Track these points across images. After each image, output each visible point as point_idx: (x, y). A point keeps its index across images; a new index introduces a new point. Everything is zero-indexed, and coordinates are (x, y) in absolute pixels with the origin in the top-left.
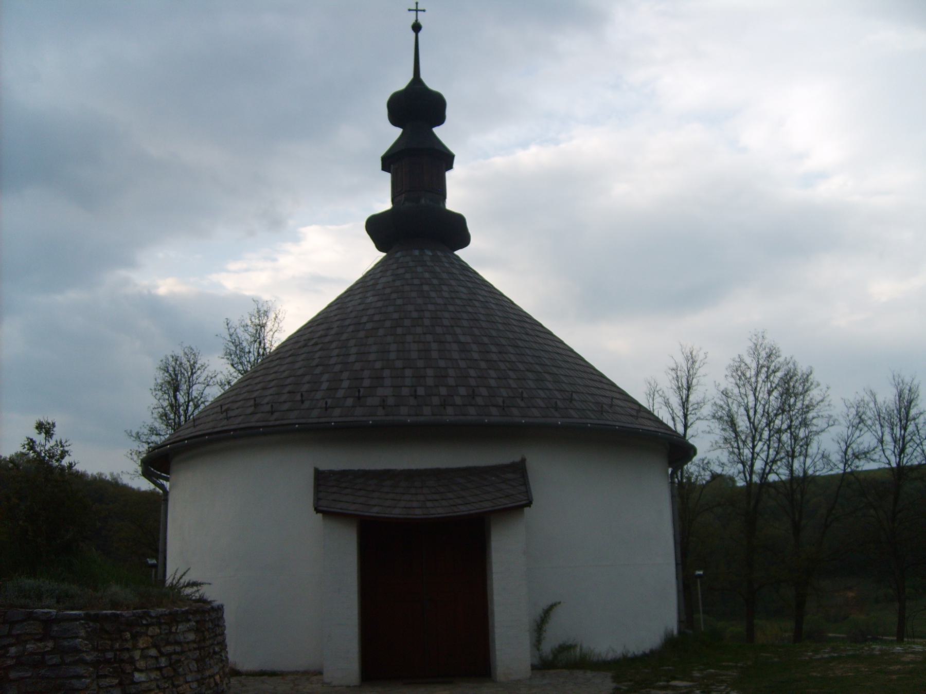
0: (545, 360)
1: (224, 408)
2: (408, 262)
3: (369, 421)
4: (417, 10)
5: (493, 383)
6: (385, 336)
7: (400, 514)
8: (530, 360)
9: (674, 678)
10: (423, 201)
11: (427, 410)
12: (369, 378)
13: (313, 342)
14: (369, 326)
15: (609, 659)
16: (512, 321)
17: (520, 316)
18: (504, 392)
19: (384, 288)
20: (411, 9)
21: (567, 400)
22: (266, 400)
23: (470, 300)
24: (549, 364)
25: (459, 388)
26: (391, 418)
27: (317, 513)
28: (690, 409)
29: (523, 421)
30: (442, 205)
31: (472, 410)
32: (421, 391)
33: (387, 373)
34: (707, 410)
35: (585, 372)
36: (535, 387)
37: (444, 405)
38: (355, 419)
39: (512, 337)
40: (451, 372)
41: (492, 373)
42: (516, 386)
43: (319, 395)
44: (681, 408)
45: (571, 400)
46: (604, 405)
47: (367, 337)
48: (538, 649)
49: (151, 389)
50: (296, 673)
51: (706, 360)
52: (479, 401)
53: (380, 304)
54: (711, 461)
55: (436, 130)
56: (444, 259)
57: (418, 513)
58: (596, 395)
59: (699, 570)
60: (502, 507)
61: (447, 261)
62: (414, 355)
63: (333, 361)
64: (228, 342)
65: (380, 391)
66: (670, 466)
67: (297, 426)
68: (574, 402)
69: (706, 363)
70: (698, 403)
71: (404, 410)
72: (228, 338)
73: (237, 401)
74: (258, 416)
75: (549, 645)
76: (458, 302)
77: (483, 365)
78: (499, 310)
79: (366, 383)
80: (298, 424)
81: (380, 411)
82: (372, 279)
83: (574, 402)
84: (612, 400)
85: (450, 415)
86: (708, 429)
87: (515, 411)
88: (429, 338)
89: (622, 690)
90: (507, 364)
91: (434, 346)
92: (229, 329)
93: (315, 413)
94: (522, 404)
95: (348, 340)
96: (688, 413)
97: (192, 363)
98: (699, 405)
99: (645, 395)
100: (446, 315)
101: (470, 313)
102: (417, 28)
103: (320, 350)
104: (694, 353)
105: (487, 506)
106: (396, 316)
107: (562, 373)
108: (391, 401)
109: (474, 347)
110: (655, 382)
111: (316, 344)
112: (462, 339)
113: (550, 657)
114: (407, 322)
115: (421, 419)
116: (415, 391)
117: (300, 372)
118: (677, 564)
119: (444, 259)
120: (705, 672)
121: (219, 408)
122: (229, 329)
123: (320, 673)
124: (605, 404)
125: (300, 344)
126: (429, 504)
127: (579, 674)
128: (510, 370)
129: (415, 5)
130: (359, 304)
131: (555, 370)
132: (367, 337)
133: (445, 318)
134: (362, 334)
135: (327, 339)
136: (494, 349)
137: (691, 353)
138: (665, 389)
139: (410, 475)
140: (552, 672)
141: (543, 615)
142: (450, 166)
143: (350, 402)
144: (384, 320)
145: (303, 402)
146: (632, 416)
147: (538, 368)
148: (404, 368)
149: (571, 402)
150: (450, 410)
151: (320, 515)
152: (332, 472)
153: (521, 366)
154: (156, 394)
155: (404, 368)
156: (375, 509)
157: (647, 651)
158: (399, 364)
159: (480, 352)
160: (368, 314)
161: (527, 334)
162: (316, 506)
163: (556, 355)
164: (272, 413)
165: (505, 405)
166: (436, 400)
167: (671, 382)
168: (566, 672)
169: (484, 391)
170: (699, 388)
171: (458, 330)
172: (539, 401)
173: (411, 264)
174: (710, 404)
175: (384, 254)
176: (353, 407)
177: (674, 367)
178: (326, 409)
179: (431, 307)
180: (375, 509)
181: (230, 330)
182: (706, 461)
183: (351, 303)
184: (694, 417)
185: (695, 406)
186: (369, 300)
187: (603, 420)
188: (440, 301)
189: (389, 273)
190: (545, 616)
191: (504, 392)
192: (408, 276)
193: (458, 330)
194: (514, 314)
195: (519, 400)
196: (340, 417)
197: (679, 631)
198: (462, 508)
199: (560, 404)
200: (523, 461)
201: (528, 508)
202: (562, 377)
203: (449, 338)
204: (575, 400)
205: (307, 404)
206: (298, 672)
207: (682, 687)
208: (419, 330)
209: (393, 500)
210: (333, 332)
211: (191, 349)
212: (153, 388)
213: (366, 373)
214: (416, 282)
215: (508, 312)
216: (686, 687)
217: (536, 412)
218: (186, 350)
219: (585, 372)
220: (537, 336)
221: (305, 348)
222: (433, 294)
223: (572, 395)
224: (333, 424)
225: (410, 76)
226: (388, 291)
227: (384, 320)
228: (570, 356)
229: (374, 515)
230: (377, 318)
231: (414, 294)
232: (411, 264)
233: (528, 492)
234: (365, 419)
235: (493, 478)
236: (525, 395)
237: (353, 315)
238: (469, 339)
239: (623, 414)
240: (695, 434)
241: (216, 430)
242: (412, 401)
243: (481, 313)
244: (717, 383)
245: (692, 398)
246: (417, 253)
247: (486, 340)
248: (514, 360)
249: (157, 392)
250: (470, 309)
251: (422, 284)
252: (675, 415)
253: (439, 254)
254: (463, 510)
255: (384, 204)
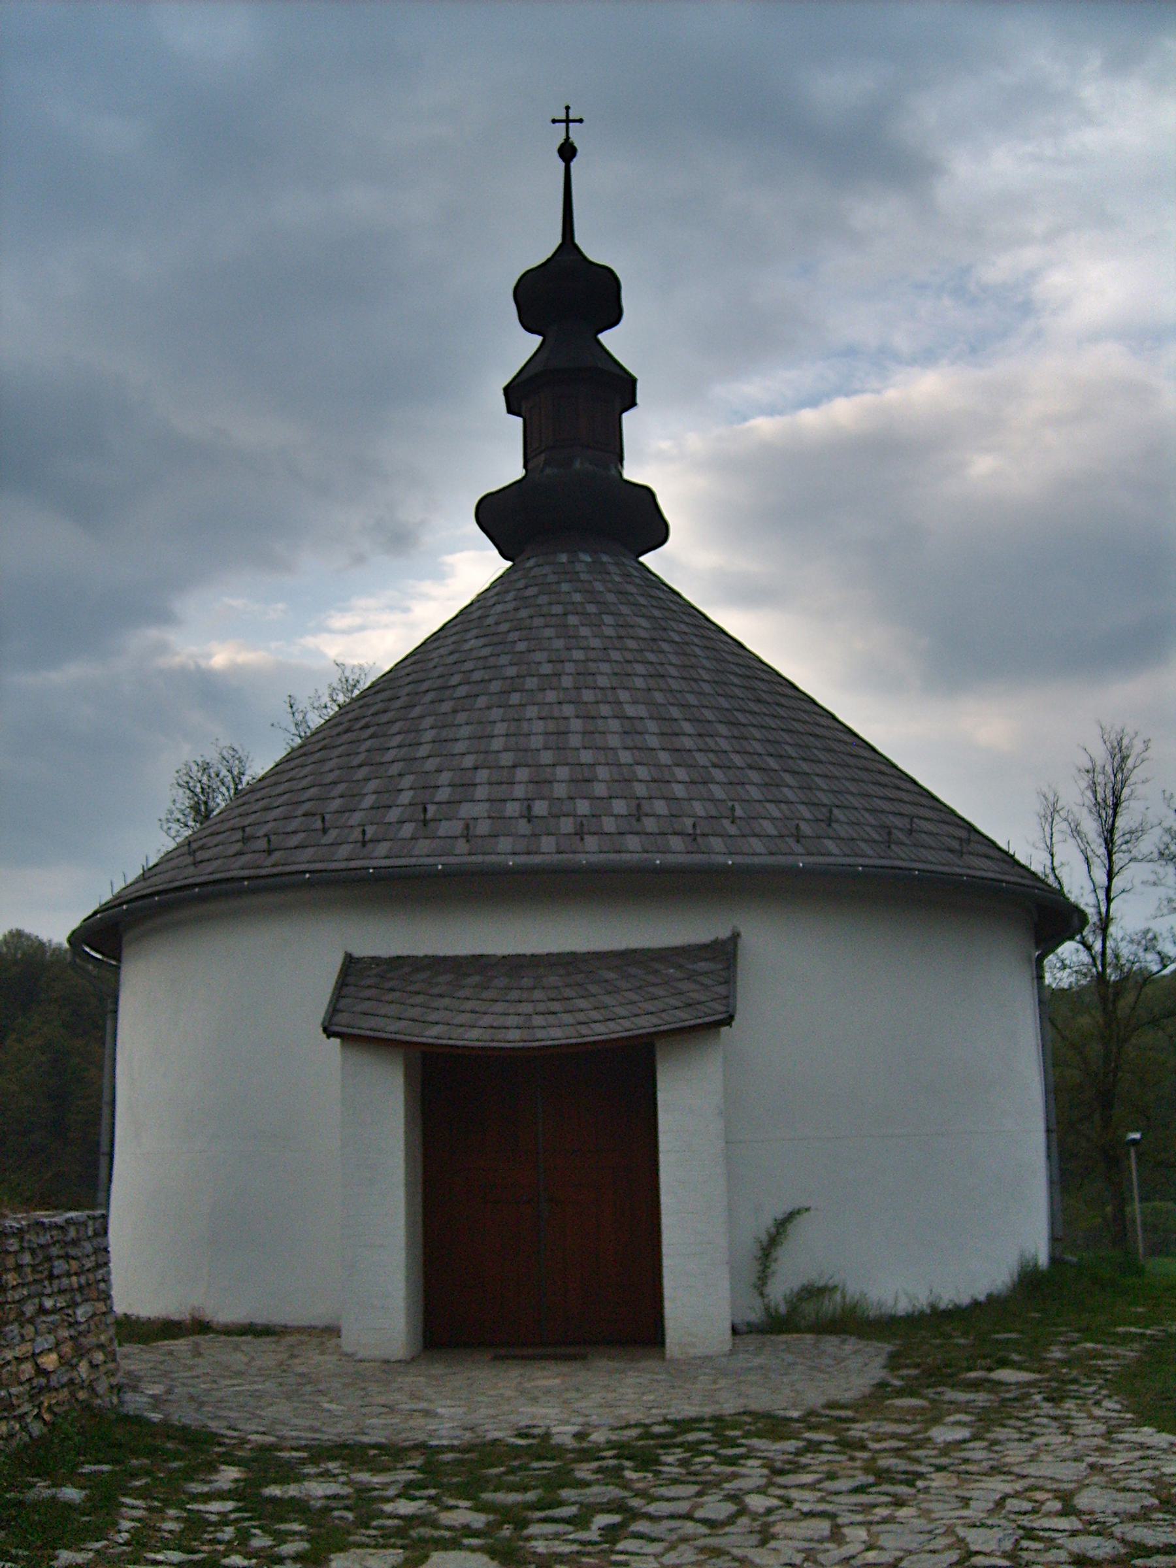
0: (816, 751)
1: (194, 846)
2: (546, 575)
3: (437, 865)
4: (567, 121)
5: (679, 790)
6: (488, 708)
7: (478, 1040)
8: (759, 748)
9: (1004, 1363)
10: (577, 465)
11: (547, 843)
12: (449, 785)
13: (363, 722)
14: (462, 691)
15: (902, 1313)
16: (732, 677)
17: (750, 667)
18: (699, 808)
19: (497, 624)
20: (578, 124)
21: (822, 821)
22: (262, 831)
23: (654, 640)
24: (794, 755)
25: (614, 801)
26: (479, 859)
27: (329, 1037)
28: (1119, 842)
29: (730, 862)
30: (613, 472)
31: (633, 842)
32: (540, 808)
33: (483, 775)
34: (1148, 844)
35: (867, 770)
36: (761, 797)
37: (580, 834)
38: (413, 861)
39: (727, 706)
40: (602, 772)
41: (681, 774)
42: (724, 797)
43: (356, 818)
44: (1101, 841)
45: (830, 821)
46: (895, 831)
47: (455, 711)
48: (762, 1294)
49: (160, 820)
50: (300, 1330)
51: (1146, 754)
52: (650, 824)
53: (486, 652)
54: (1158, 934)
55: (604, 337)
56: (612, 569)
57: (514, 1037)
58: (883, 812)
59: (1136, 1130)
60: (678, 1025)
61: (618, 572)
62: (536, 742)
63: (389, 756)
64: (292, 737)
65: (466, 810)
66: (1037, 948)
67: (307, 875)
68: (834, 825)
69: (1148, 759)
70: (1131, 833)
71: (505, 844)
72: (293, 729)
73: (218, 833)
74: (244, 859)
75: (780, 1289)
76: (631, 644)
77: (664, 757)
78: (707, 658)
79: (443, 794)
80: (309, 872)
81: (462, 846)
82: (480, 608)
83: (834, 825)
84: (911, 820)
85: (591, 852)
86: (1152, 878)
87: (717, 843)
88: (568, 710)
89: (889, 1389)
90: (711, 756)
91: (576, 725)
92: (293, 714)
93: (344, 851)
94: (732, 830)
95: (422, 717)
96: (1115, 849)
97: (236, 773)
98: (1134, 834)
99: (1036, 819)
100: (605, 667)
101: (652, 663)
102: (567, 152)
103: (371, 737)
104: (1125, 742)
105: (645, 1024)
106: (512, 671)
107: (847, 775)
108: (483, 828)
109: (652, 726)
110: (1055, 795)
111: (366, 726)
112: (630, 711)
113: (783, 1309)
114: (531, 683)
115: (537, 859)
116: (529, 808)
117: (330, 778)
118: (1048, 1131)
119: (612, 569)
120: (1073, 1349)
121: (186, 847)
122: (293, 714)
123: (333, 1331)
124: (896, 828)
125: (340, 728)
126: (538, 1021)
127: (830, 1343)
128: (715, 766)
129: (564, 111)
130: (451, 653)
131: (805, 767)
132: (455, 711)
133: (602, 674)
134: (446, 707)
135: (385, 718)
136: (687, 727)
137: (1120, 742)
138: (1075, 809)
139: (516, 965)
140: (784, 1337)
141: (773, 1230)
142: (631, 402)
143: (408, 830)
144: (490, 680)
145: (325, 831)
146: (951, 851)
147: (772, 763)
148: (514, 766)
149: (829, 825)
150: (591, 842)
151: (335, 1042)
152: (376, 960)
153: (738, 760)
154: (169, 828)
155: (514, 766)
156: (435, 1031)
157: (982, 1298)
158: (507, 759)
159: (662, 734)
160: (462, 669)
161: (759, 701)
162: (326, 1024)
163: (811, 739)
164: (270, 852)
165: (698, 832)
166: (567, 825)
167: (1083, 793)
168: (809, 1338)
169: (660, 807)
170: (1133, 804)
171: (623, 696)
172: (766, 824)
173: (552, 578)
174: (1158, 831)
175: (509, 564)
176: (412, 839)
177: (1089, 766)
178: (364, 843)
179: (578, 655)
180: (435, 1031)
181: (296, 714)
182: (1150, 935)
183: (438, 651)
184: (1127, 857)
185: (1127, 837)
186: (467, 646)
187: (890, 858)
188: (596, 643)
189: (511, 595)
190: (778, 1233)
191: (699, 808)
192: (543, 600)
193: (623, 696)
194: (738, 665)
195: (726, 823)
196: (387, 857)
197: (1054, 1260)
198: (599, 1028)
199: (805, 828)
200: (736, 936)
201: (728, 1027)
202: (816, 779)
203: (605, 710)
204: (837, 821)
205: (333, 834)
206: (315, 1328)
207: (1011, 1384)
208: (551, 696)
209: (473, 1012)
210: (398, 704)
211: (234, 750)
212: (163, 818)
213: (445, 778)
214: (557, 609)
215: (725, 661)
216: (1018, 1384)
217: (757, 845)
218: (225, 754)
219: (867, 770)
220: (778, 704)
221: (349, 734)
222: (584, 631)
223: (831, 812)
224: (371, 871)
225: (555, 240)
226: (504, 627)
227: (490, 680)
228: (840, 741)
229: (431, 1041)
230: (477, 676)
231: (549, 632)
232: (552, 578)
233: (729, 999)
234: (431, 860)
235: (672, 971)
236: (739, 812)
237: (436, 673)
238: (642, 711)
239: (931, 848)
240: (1129, 887)
241: (177, 884)
242: (523, 827)
243: (671, 664)
244: (1167, 795)
245: (1121, 823)
246: (563, 558)
247: (675, 712)
248: (724, 749)
249: (170, 824)
250: (651, 657)
251: (565, 614)
252: (1090, 854)
253: (605, 558)
254: (602, 1031)
255: (511, 469)
